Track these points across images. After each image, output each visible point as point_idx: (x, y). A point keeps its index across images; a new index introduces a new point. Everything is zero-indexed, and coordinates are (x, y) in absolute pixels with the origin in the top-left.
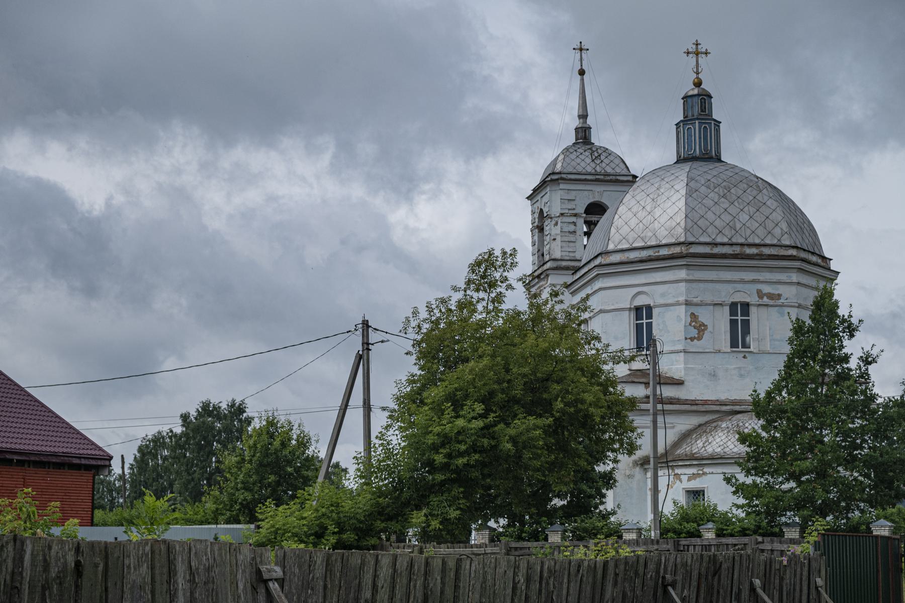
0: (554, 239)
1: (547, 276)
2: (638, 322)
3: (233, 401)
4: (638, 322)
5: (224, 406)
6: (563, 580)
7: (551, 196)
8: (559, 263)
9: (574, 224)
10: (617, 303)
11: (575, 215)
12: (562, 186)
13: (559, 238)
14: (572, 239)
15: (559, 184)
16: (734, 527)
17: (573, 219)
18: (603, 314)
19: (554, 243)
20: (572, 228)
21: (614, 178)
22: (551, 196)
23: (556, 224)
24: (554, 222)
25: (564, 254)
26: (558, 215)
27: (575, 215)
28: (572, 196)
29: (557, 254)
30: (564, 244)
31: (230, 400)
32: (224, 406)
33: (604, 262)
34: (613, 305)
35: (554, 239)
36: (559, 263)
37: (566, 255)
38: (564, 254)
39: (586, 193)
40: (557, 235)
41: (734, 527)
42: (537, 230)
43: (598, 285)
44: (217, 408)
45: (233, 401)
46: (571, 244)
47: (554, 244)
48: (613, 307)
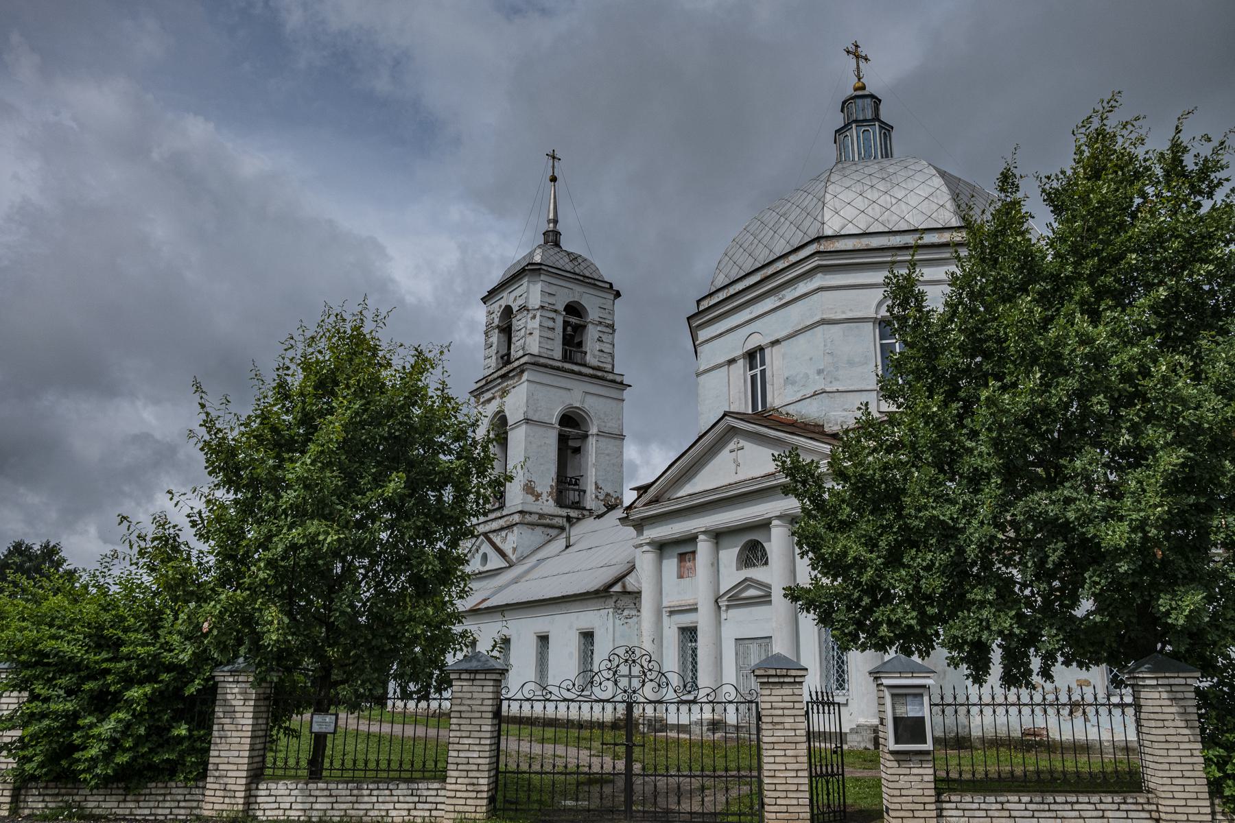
0: (531, 334)
1: (522, 372)
2: (884, 342)
3: (48, 542)
4: (884, 342)
5: (36, 547)
6: (570, 809)
7: (528, 287)
8: (537, 359)
9: (553, 319)
10: (851, 310)
11: (555, 311)
12: (543, 277)
13: (537, 333)
14: (551, 336)
15: (540, 274)
16: (21, 753)
17: (553, 315)
18: (825, 326)
19: (531, 337)
20: (551, 324)
21: (593, 281)
22: (528, 287)
23: (534, 317)
24: (530, 315)
25: (542, 350)
26: (537, 307)
27: (555, 311)
28: (552, 290)
29: (535, 350)
30: (542, 339)
31: (45, 541)
32: (36, 547)
33: (822, 248)
34: (844, 312)
35: (531, 334)
36: (537, 359)
37: (545, 353)
38: (542, 350)
39: (566, 290)
40: (534, 329)
41: (21, 753)
42: (497, 331)
43: (819, 281)
44: (29, 548)
45: (48, 542)
46: (549, 341)
47: (529, 339)
48: (844, 316)
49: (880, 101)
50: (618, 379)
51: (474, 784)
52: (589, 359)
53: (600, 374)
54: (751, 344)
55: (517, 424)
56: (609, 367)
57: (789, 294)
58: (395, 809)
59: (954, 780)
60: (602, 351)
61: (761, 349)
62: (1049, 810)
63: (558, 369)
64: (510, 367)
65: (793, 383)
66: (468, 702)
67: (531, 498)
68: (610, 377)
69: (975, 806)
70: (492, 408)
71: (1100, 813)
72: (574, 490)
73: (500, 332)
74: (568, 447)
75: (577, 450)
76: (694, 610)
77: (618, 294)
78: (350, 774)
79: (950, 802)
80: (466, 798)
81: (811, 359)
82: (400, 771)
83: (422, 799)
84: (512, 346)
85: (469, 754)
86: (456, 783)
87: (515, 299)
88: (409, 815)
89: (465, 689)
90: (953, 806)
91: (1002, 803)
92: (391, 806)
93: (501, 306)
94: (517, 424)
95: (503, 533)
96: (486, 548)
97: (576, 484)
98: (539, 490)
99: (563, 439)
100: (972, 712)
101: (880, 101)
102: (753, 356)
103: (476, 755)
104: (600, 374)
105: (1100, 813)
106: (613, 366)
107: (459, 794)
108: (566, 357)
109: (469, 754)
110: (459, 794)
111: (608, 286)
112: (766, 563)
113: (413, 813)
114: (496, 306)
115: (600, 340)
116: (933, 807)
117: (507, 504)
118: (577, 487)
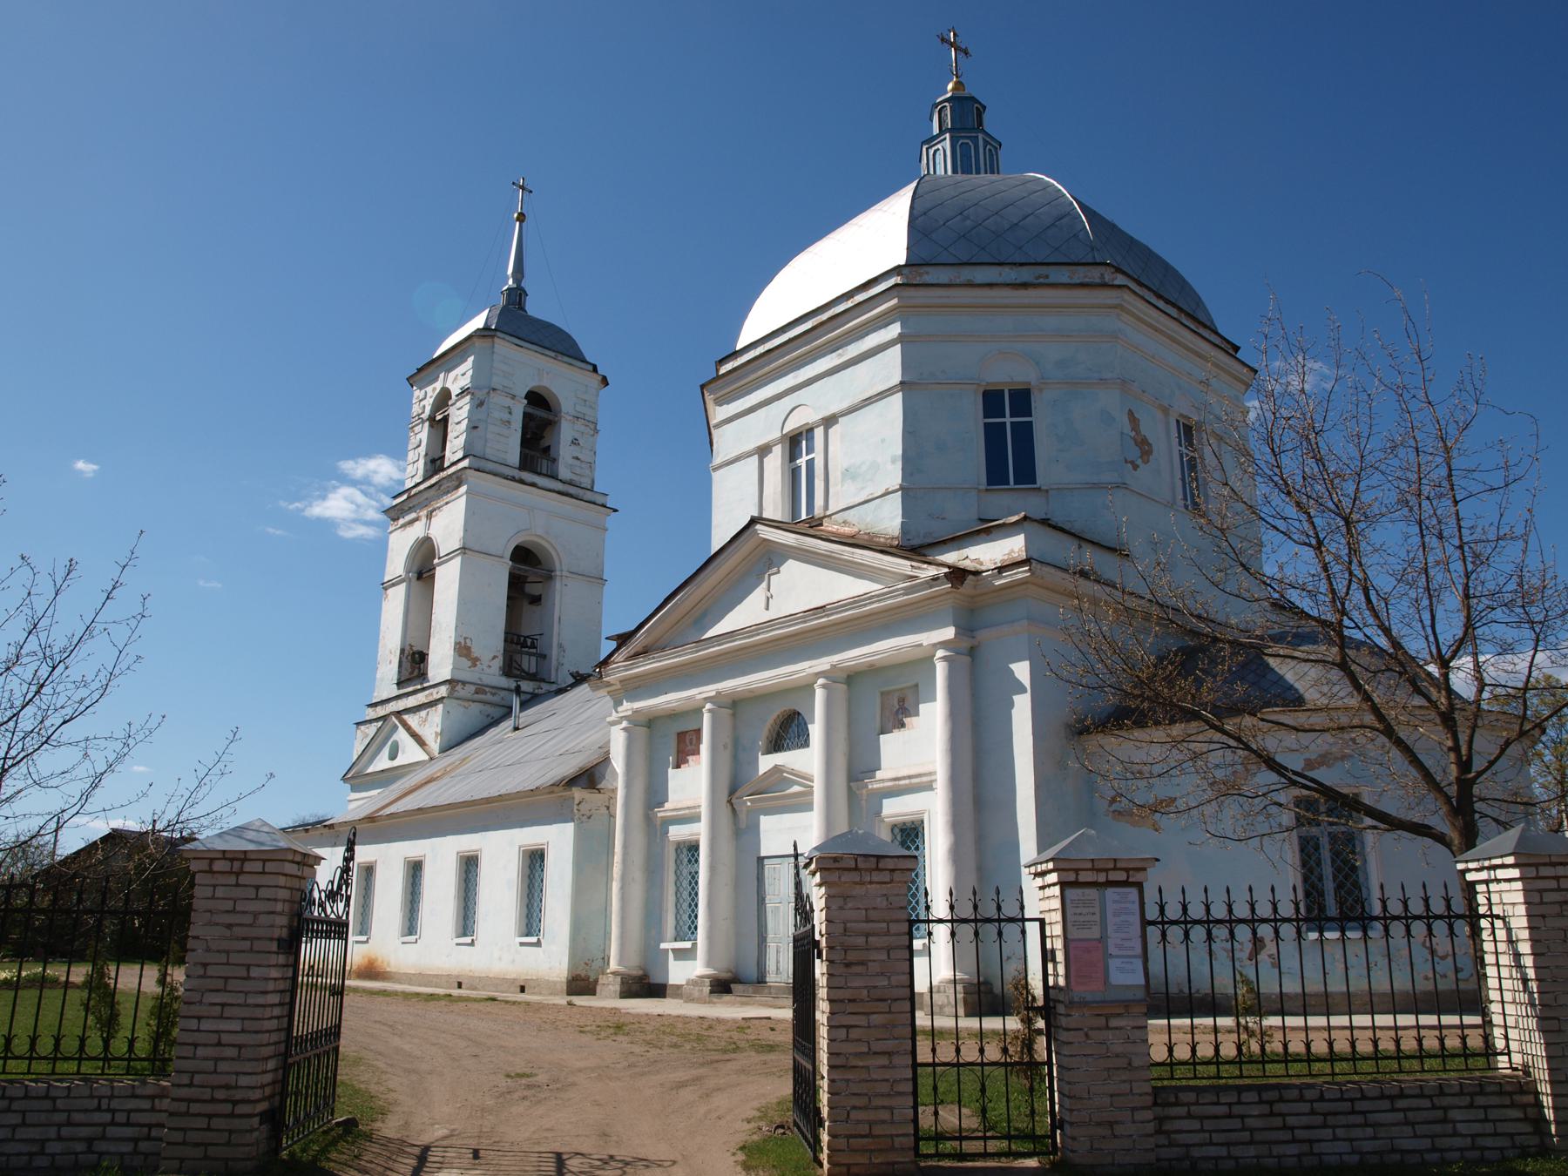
11: (513, 397)
27: (513, 397)
49: (984, 108)
50: (600, 500)
51: (227, 1087)
52: (564, 473)
53: (572, 490)
54: (791, 425)
55: (450, 555)
56: (586, 482)
57: (853, 350)
58: (60, 1138)
59: (1297, 1059)
60: (577, 458)
61: (809, 431)
62: (1353, 1112)
63: (513, 479)
64: (443, 474)
65: (854, 478)
66: (885, 1102)
67: (466, 663)
68: (589, 496)
69: (1223, 1110)
70: (417, 531)
71: (1439, 1114)
72: (530, 654)
73: (431, 426)
74: (522, 591)
75: (536, 600)
76: (699, 835)
77: (605, 381)
78: (72, 1067)
79: (1177, 1104)
80: (210, 1116)
81: (883, 441)
82: (31, 1059)
83: (121, 1118)
84: (448, 444)
85: (224, 1025)
86: (191, 1085)
87: (455, 379)
88: (90, 1151)
89: (220, 892)
90: (1182, 1111)
91: (1271, 1103)
92: (52, 1133)
93: (434, 389)
94: (450, 555)
95: (423, 713)
96: (401, 735)
97: (533, 646)
98: (476, 653)
99: (516, 584)
100: (1192, 936)
101: (984, 108)
102: (795, 442)
103: (236, 1026)
104: (572, 490)
105: (1439, 1114)
106: (593, 482)
107: (195, 1108)
108: (527, 463)
109: (224, 1025)
110: (195, 1108)
111: (591, 368)
112: (808, 746)
113: (102, 1146)
114: (429, 389)
115: (575, 442)
116: (1149, 1115)
117: (430, 674)
118: (534, 651)
